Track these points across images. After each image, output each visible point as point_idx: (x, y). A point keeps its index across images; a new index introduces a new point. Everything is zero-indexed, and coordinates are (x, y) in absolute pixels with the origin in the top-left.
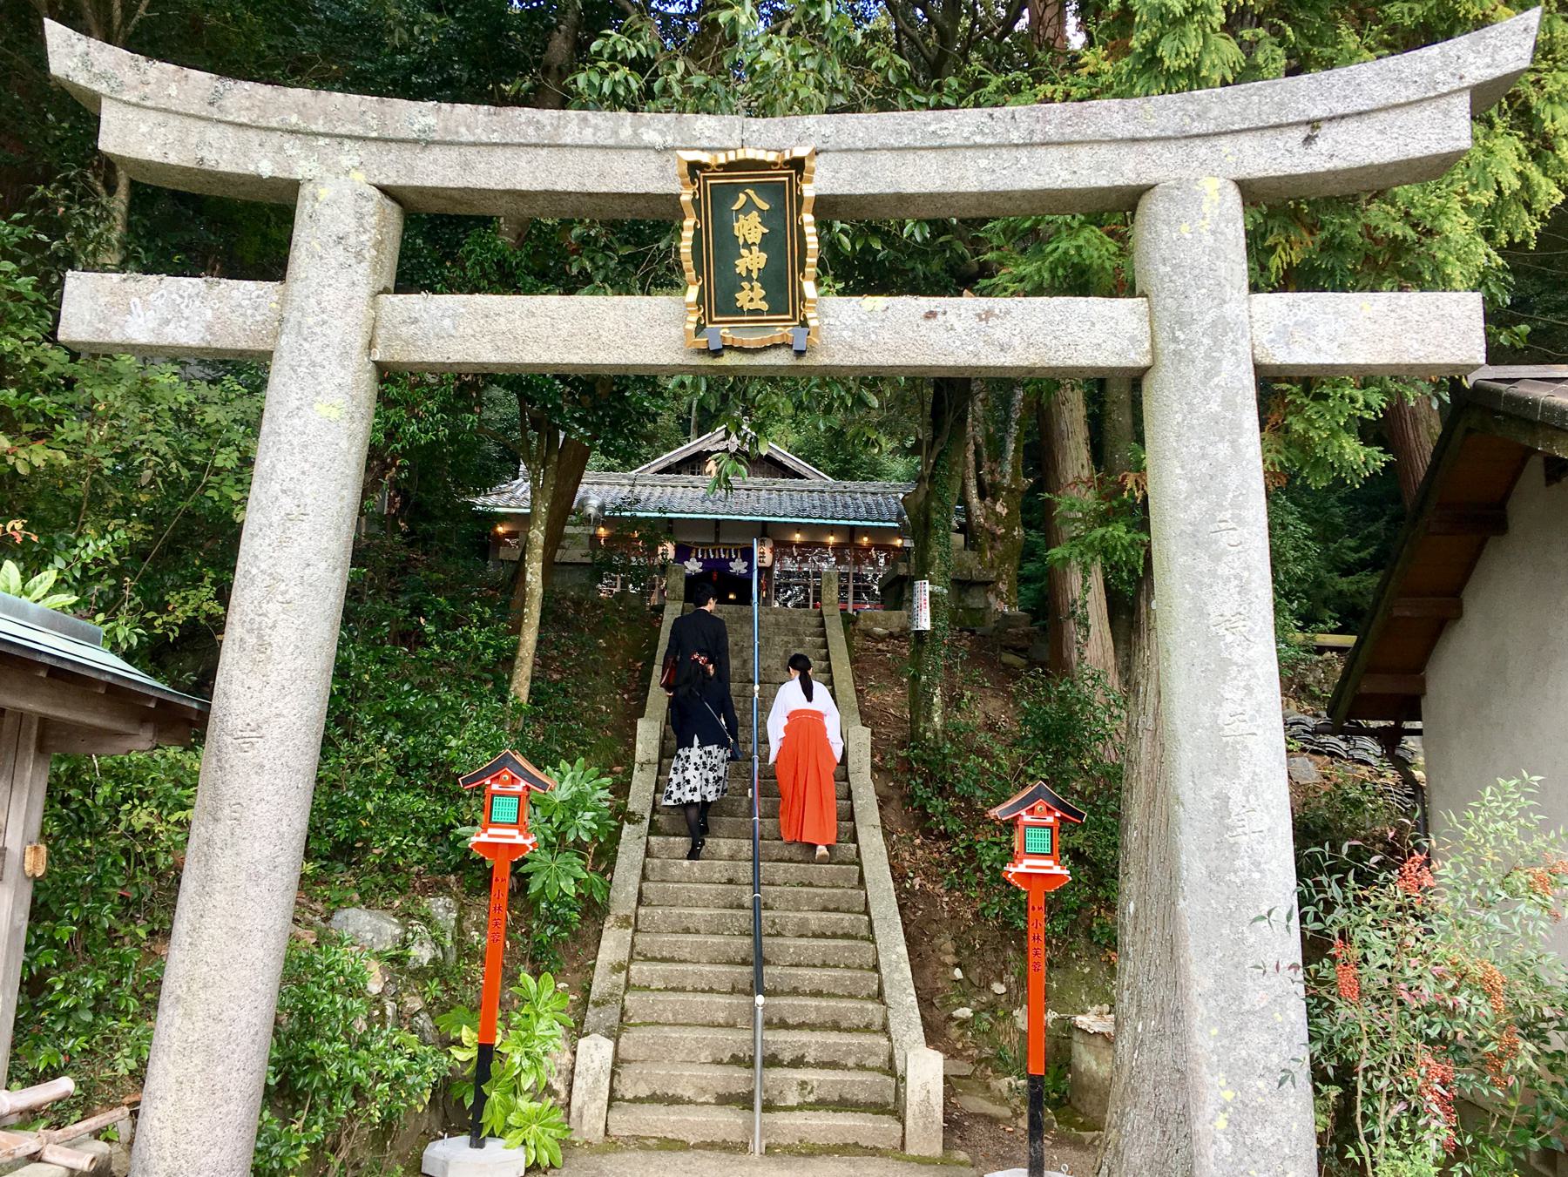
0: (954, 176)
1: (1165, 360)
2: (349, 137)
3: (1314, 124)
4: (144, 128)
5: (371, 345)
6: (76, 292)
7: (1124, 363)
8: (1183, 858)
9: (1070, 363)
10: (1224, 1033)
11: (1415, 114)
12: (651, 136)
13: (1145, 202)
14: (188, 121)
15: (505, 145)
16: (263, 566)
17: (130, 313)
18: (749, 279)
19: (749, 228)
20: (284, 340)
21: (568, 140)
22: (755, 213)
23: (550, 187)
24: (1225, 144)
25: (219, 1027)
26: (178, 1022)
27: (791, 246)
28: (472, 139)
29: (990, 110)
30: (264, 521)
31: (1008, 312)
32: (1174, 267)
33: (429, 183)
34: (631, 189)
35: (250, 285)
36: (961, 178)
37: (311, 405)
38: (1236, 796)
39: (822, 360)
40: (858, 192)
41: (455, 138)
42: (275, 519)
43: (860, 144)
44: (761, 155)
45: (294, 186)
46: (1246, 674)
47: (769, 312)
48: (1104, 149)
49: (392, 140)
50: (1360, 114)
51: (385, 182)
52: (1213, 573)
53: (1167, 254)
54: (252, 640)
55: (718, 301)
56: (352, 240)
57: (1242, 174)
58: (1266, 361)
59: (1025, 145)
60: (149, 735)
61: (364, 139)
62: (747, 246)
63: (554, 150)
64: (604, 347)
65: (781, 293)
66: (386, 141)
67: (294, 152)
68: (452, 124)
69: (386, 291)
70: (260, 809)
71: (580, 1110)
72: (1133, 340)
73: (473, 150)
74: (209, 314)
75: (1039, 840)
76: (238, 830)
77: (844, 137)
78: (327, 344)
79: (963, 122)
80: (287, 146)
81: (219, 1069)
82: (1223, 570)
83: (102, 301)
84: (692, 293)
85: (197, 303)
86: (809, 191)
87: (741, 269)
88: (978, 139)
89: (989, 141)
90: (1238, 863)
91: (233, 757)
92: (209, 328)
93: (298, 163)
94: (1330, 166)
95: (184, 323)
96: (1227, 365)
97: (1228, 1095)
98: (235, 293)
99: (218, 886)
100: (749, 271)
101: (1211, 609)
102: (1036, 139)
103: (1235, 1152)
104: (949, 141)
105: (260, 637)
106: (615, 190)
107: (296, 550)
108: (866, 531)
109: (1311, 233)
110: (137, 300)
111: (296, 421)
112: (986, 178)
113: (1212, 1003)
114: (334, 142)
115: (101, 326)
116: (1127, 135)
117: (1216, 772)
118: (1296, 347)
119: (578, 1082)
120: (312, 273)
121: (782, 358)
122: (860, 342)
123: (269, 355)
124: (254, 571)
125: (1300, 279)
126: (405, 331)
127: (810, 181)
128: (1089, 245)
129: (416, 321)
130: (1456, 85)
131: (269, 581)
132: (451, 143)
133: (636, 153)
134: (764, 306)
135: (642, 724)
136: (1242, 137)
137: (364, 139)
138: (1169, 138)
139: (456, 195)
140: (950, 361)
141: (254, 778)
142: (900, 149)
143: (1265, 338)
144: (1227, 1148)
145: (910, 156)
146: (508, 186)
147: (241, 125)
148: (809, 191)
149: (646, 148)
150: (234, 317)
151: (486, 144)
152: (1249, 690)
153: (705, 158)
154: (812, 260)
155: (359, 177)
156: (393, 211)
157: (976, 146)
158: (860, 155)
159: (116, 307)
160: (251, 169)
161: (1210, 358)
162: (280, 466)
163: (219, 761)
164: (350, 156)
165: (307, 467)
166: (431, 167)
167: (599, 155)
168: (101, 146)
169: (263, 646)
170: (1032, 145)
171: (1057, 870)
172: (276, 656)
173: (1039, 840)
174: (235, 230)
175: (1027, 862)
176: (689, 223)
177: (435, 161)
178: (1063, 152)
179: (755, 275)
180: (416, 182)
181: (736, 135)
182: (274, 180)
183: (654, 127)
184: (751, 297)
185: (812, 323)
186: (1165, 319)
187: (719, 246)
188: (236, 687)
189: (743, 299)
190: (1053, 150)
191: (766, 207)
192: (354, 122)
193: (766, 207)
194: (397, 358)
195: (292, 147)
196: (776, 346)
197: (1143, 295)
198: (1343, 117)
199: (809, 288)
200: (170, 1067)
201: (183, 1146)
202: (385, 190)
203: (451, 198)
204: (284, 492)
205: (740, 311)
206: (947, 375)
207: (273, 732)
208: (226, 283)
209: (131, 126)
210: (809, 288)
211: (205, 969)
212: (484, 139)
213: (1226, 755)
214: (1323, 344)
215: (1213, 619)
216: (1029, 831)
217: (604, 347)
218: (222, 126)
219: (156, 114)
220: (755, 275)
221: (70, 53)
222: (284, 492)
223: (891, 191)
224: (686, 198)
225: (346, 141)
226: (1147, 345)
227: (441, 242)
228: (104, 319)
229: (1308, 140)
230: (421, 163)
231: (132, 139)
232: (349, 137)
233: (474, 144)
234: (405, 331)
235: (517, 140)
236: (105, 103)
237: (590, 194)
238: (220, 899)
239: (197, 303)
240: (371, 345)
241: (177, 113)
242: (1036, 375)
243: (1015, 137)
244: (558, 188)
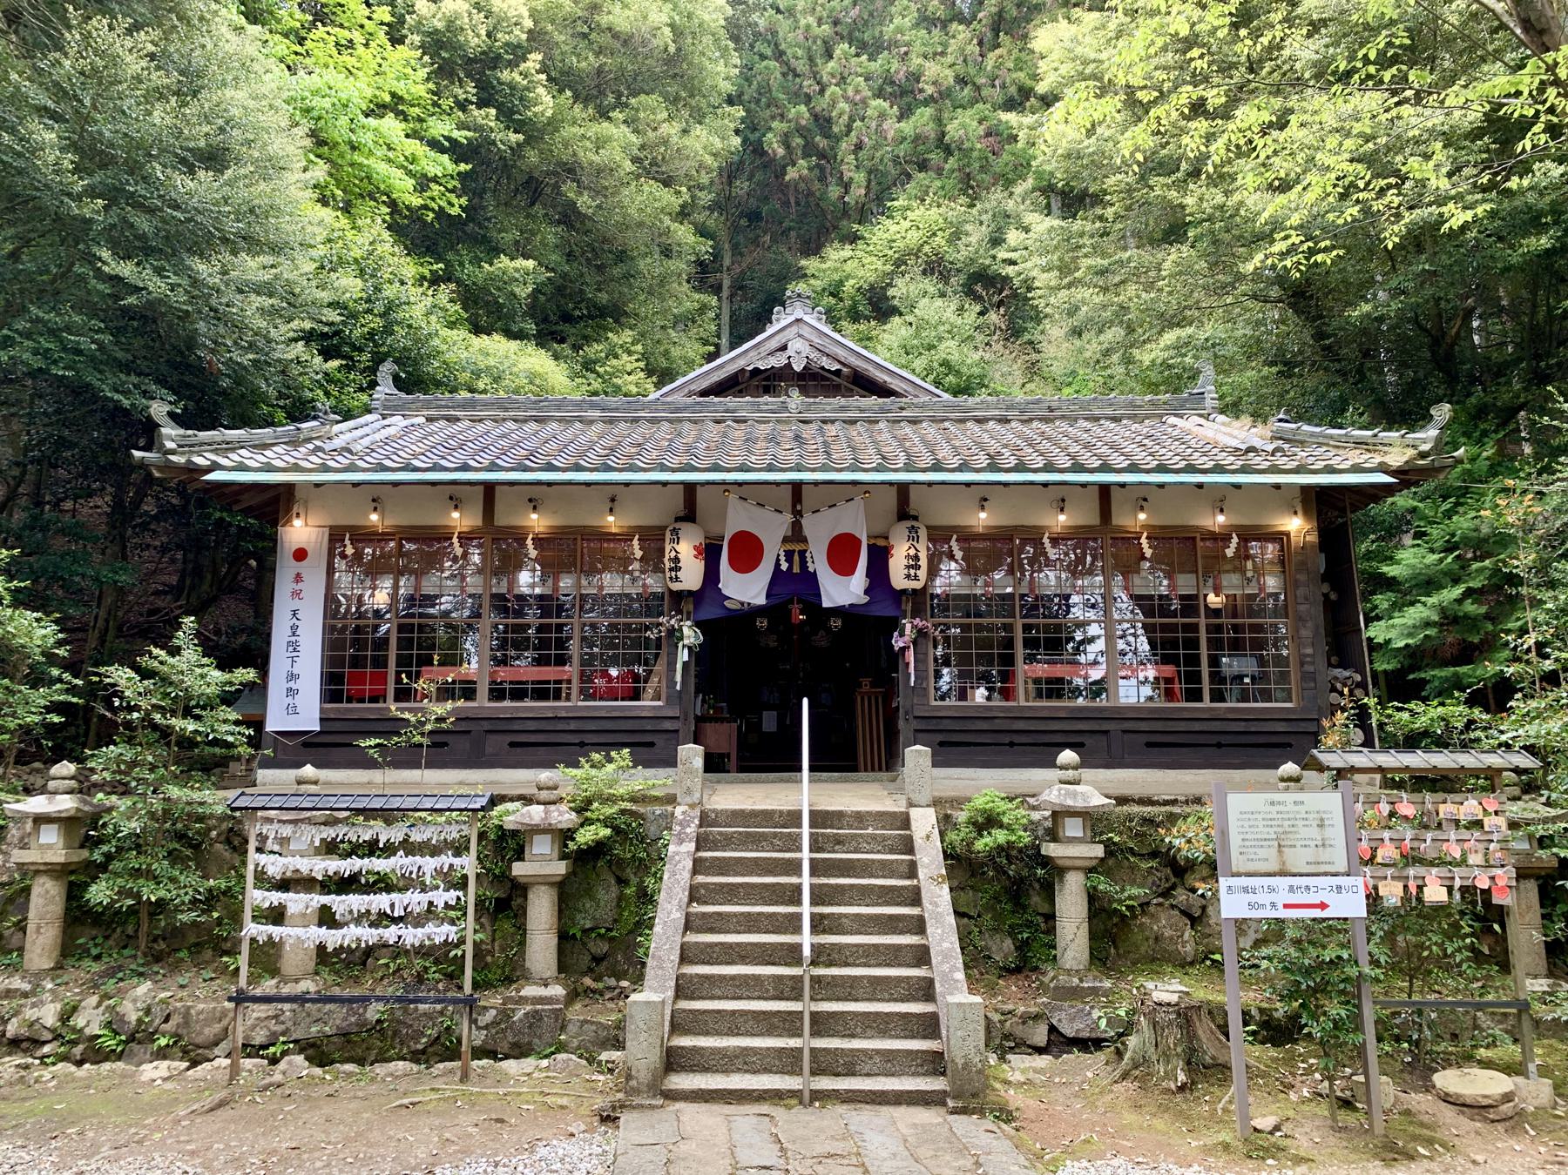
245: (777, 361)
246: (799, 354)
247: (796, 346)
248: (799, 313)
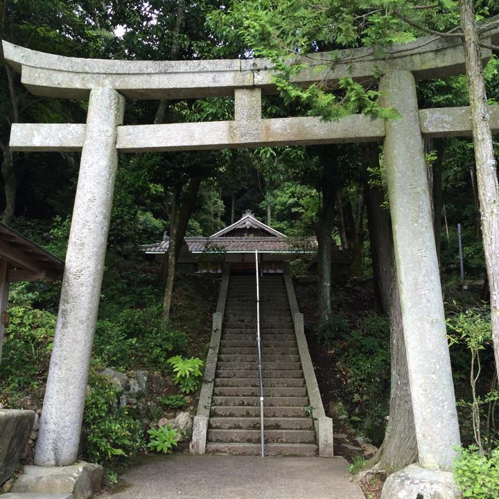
5: (116, 143)
20: (86, 142)
23: (176, 87)
25: (71, 373)
26: (56, 372)
33: (134, 88)
34: (203, 86)
45: (88, 91)
51: (119, 88)
60: (44, 274)
69: (120, 125)
70: (83, 298)
78: (97, 142)
81: (71, 387)
93: (89, 86)
123: (82, 147)
125: (233, 113)
135: (215, 315)
156: (122, 99)
159: (24, 135)
167: (191, 75)
174: (71, 107)
177: (136, 80)
201: (59, 414)
203: (141, 93)
206: (316, 144)
219: (40, 69)
221: (12, 52)
226: (384, 129)
227: (140, 108)
236: (23, 67)
238: (70, 329)
242: (347, 142)
244: (178, 87)
245: (244, 226)
246: (248, 225)
247: (247, 223)
248: (248, 216)
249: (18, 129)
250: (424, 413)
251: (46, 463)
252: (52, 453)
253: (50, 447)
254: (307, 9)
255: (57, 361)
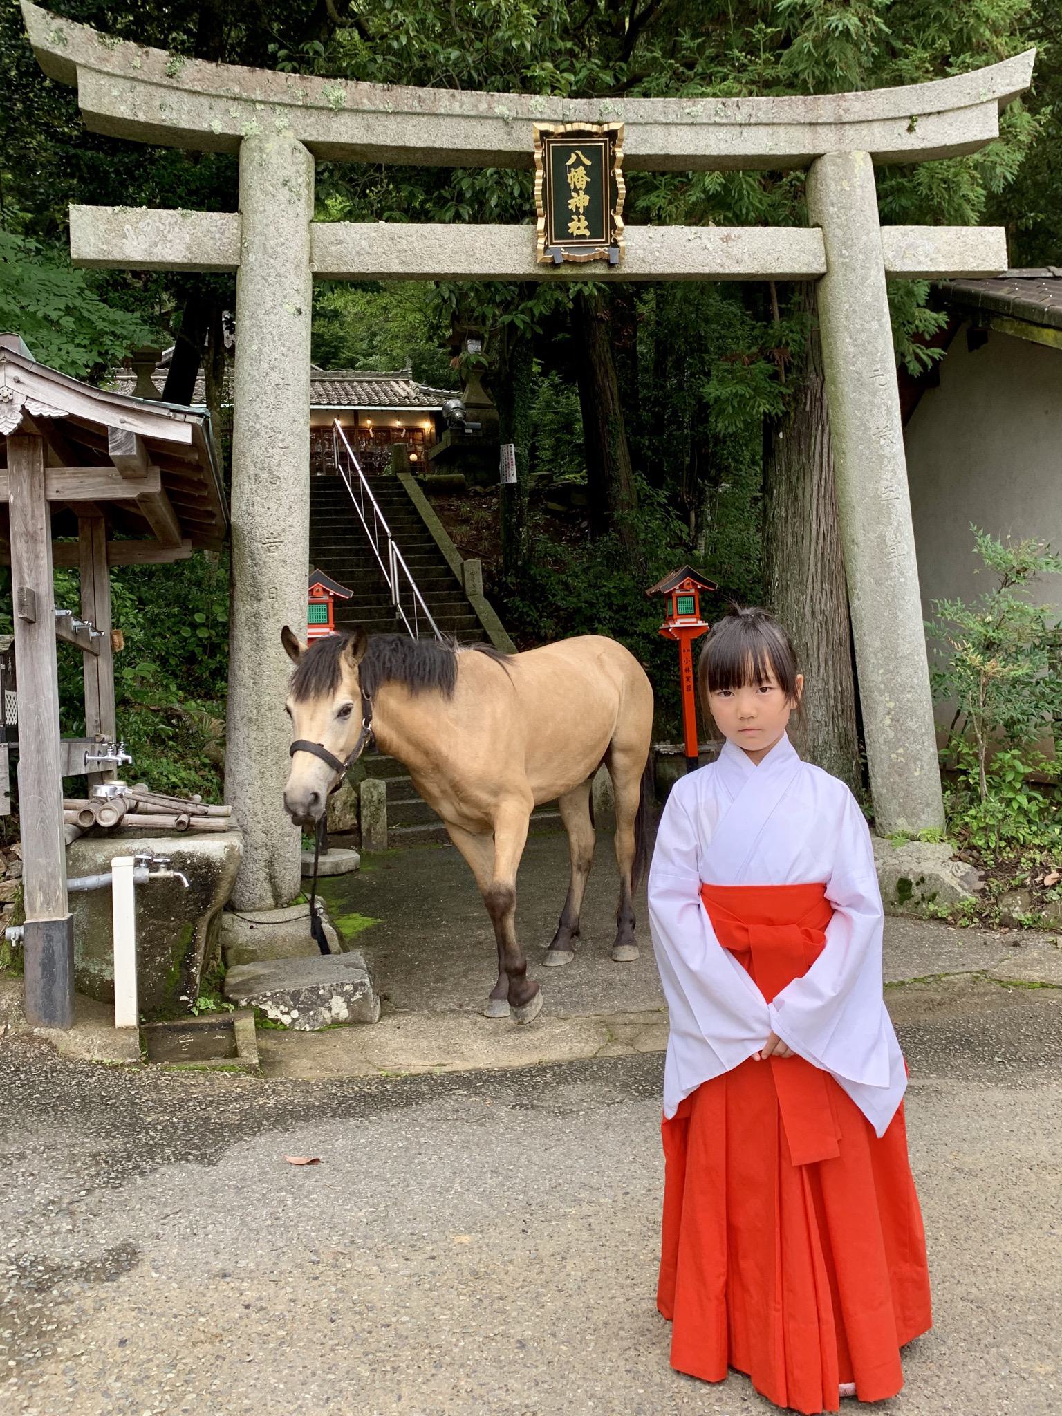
0: (702, 144)
1: (836, 268)
2: (279, 104)
3: (913, 118)
4: (115, 93)
6: (80, 221)
7: (811, 271)
8: (858, 576)
9: (779, 271)
10: (887, 671)
11: (968, 112)
12: (500, 109)
13: (819, 165)
14: (152, 89)
15: (398, 113)
16: (265, 423)
17: (126, 237)
18: (578, 213)
19: (578, 178)
20: (252, 258)
21: (443, 111)
22: (582, 167)
23: (431, 145)
24: (864, 129)
26: (253, 734)
27: (606, 193)
28: (373, 108)
29: (724, 100)
30: (258, 390)
31: (739, 237)
32: (839, 209)
33: (342, 140)
34: (488, 147)
35: (215, 215)
36: (707, 146)
37: (281, 305)
38: (890, 535)
39: (625, 270)
40: (641, 153)
41: (360, 107)
42: (269, 389)
43: (641, 120)
44: (588, 127)
45: (238, 140)
46: (892, 463)
47: (590, 237)
48: (792, 129)
49: (311, 107)
50: (939, 113)
52: (872, 403)
53: (834, 200)
54: (264, 475)
55: (558, 230)
56: (293, 182)
57: (874, 149)
58: (891, 269)
59: (746, 125)
61: (291, 106)
62: (576, 190)
63: (433, 118)
64: (477, 261)
65: (599, 226)
66: (308, 108)
67: (238, 114)
68: (357, 97)
70: (289, 590)
71: (369, 831)
72: (815, 255)
73: (374, 116)
74: (187, 238)
75: (686, 605)
76: (276, 606)
77: (630, 115)
79: (704, 107)
80: (231, 109)
82: (877, 400)
83: (102, 228)
84: (541, 223)
85: (177, 229)
86: (620, 154)
87: (572, 207)
88: (717, 119)
89: (724, 121)
90: (892, 574)
91: (265, 557)
92: (188, 249)
93: (245, 124)
94: (923, 145)
95: (169, 245)
96: (873, 272)
97: (891, 705)
98: (204, 222)
99: (269, 644)
100: (577, 208)
101: (872, 425)
102: (753, 121)
103: (896, 735)
104: (699, 120)
105: (270, 473)
106: (476, 148)
107: (286, 410)
108: (369, 414)
109: (908, 190)
110: (128, 227)
111: (272, 317)
112: (722, 146)
113: (880, 655)
114: (268, 108)
115: (105, 247)
116: (808, 121)
117: (879, 523)
118: (906, 261)
119: (365, 812)
120: (269, 207)
121: (600, 270)
122: (649, 258)
124: (258, 426)
126: (335, 249)
127: (620, 146)
128: (782, 190)
129: (341, 243)
130: (991, 96)
131: (270, 433)
132: (357, 111)
133: (490, 122)
134: (587, 233)
136: (875, 125)
137: (291, 106)
138: (830, 124)
139: (358, 148)
140: (706, 271)
141: (282, 570)
142: (667, 124)
143: (890, 254)
144: (892, 734)
145: (673, 129)
146: (400, 143)
147: (195, 93)
148: (620, 154)
149: (497, 118)
150: (206, 240)
151: (382, 112)
152: (894, 471)
153: (550, 127)
154: (621, 201)
155: (290, 138)
157: (716, 124)
158: (640, 128)
159: (104, 233)
160: (205, 127)
161: (862, 259)
162: (266, 350)
163: (253, 560)
164: (281, 119)
165: (285, 350)
166: (343, 128)
167: (463, 122)
168: (80, 105)
169: (274, 479)
170: (750, 125)
171: (700, 623)
172: (283, 485)
173: (685, 605)
174: (208, 175)
175: (679, 621)
176: (539, 173)
177: (345, 123)
178: (769, 129)
179: (581, 211)
180: (331, 139)
181: (560, 110)
182: (223, 135)
183: (505, 103)
184: (578, 226)
185: (621, 244)
186: (835, 244)
187: (560, 190)
188: (257, 508)
189: (573, 227)
190: (762, 128)
191: (589, 163)
192: (285, 92)
193: (589, 163)
194: (330, 270)
195: (235, 110)
196: (595, 261)
197: (817, 225)
198: (930, 114)
199: (619, 220)
200: (252, 764)
202: (307, 144)
204: (272, 369)
205: (571, 236)
207: (288, 538)
208: (196, 215)
209: (105, 89)
210: (619, 220)
211: (268, 698)
212: (381, 108)
213: (882, 510)
214: (922, 258)
215: (873, 430)
216: (680, 600)
217: (477, 261)
218: (179, 93)
219: (119, 82)
220: (581, 211)
222: (272, 369)
223: (662, 152)
224: (538, 156)
225: (277, 107)
226: (823, 259)
228: (106, 242)
229: (910, 129)
230: (335, 125)
231: (106, 101)
232: (279, 104)
233: (374, 112)
234: (335, 249)
235: (406, 109)
236: (79, 71)
237: (458, 150)
239: (177, 229)
240: (311, 261)
241: (142, 81)
243: (740, 119)
249: (86, 218)
250: (893, 756)
251: (258, 906)
252: (267, 886)
253: (262, 875)
254: (430, 339)
255: (254, 715)
